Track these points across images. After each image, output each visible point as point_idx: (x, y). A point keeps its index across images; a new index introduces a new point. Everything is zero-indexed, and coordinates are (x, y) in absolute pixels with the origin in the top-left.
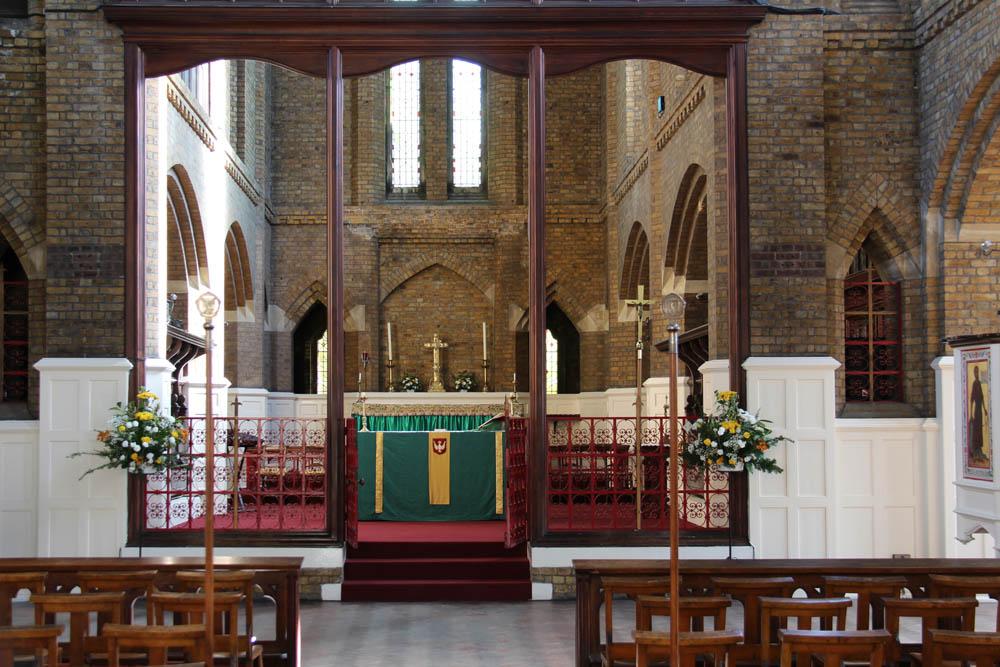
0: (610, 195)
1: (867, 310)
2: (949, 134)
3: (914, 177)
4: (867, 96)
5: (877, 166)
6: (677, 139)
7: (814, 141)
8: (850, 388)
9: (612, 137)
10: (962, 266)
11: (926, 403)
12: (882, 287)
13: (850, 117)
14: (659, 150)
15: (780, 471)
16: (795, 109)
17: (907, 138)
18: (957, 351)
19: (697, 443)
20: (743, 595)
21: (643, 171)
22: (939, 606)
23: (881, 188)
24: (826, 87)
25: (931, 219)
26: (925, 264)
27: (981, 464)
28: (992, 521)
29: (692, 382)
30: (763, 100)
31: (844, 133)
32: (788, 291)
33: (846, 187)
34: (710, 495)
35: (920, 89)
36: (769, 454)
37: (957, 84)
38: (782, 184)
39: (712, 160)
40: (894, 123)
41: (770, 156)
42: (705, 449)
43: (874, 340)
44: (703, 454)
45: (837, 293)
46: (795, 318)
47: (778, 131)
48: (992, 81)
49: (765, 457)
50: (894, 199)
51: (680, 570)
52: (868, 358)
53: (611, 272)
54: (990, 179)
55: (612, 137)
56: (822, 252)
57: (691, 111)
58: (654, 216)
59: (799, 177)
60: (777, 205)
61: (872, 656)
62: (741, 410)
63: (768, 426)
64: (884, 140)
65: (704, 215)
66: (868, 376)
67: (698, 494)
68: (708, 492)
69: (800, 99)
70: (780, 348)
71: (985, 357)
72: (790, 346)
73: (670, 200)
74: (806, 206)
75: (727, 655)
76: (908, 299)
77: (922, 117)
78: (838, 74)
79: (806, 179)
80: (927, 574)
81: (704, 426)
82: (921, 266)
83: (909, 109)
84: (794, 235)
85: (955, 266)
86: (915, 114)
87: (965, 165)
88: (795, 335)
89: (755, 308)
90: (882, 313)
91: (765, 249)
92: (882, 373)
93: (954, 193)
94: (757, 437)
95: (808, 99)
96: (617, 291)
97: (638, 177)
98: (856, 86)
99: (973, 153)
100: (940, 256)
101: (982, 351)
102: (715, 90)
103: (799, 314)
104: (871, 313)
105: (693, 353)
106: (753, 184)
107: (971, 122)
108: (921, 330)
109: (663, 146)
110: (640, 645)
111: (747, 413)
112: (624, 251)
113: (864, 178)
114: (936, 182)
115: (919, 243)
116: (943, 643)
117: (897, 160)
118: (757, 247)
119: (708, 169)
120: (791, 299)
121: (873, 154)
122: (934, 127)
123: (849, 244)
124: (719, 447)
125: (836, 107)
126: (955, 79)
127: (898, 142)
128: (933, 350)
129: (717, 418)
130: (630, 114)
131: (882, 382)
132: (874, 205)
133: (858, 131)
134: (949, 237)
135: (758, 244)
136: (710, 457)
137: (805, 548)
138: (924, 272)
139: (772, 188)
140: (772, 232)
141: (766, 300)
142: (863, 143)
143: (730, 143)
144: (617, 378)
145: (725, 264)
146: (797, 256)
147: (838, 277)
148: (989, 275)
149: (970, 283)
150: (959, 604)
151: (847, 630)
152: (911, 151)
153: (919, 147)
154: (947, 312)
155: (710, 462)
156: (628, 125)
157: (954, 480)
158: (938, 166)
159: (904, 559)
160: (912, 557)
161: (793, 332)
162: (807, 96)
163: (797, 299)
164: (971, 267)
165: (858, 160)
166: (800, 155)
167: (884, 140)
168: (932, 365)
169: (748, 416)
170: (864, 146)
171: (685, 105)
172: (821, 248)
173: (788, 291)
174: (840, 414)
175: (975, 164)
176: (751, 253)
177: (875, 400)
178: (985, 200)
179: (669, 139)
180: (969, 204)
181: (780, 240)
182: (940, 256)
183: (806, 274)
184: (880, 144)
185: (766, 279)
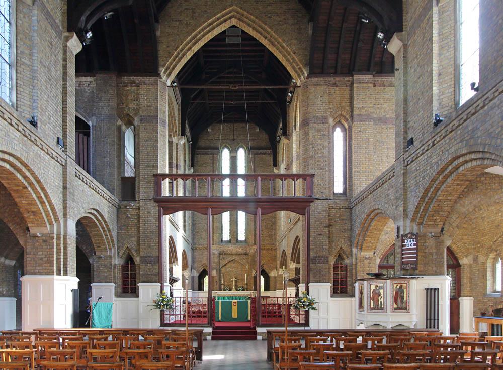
3: (350, 239)
6: (293, 230)
25: (354, 250)
36: (314, 306)
64: (343, 231)
73: (292, 245)
74: (324, 247)
85: (360, 261)
100: (356, 259)
108: (352, 277)
119: (301, 237)
131: (341, 289)
134: (358, 254)
152: (349, 233)
167: (343, 231)
172: (327, 257)
174: (332, 297)
182: (356, 259)
183: (324, 263)
185: (314, 265)
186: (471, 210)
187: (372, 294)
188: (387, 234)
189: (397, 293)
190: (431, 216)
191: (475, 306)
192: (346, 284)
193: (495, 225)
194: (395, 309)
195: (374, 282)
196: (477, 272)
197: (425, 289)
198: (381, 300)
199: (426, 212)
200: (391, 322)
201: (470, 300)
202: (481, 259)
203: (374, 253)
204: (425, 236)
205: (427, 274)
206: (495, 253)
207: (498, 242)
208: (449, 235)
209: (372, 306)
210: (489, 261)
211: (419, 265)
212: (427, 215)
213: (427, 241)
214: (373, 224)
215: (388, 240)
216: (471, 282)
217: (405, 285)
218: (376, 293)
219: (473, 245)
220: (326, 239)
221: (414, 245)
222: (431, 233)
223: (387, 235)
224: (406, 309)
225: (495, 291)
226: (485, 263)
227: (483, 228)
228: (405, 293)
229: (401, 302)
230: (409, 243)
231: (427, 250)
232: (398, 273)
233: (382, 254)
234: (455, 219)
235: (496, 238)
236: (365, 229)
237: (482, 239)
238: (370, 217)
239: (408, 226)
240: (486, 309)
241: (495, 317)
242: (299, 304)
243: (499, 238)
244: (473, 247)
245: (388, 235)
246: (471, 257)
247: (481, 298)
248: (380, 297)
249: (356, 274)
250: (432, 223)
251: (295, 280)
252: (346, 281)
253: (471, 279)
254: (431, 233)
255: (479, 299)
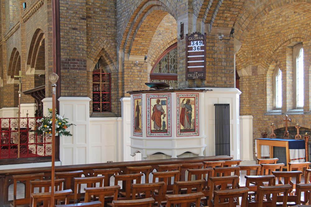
0: (3, 37)
1: (100, 82)
2: (126, 26)
3: (115, 37)
4: (100, 11)
5: (103, 34)
6: (32, 19)
7: (83, 24)
8: (94, 107)
9: (4, 15)
10: (130, 69)
11: (118, 112)
12: (104, 75)
13: (95, 17)
14: (24, 22)
15: (71, 135)
16: (76, 13)
17: (113, 26)
18: (131, 95)
19: (41, 126)
20: (24, 182)
21: (17, 29)
22: (132, 176)
23: (105, 42)
24: (87, 6)
25: (120, 53)
26: (118, 68)
27: (138, 131)
28: (142, 149)
29: (37, 105)
30: (65, 8)
31: (93, 23)
32: (74, 75)
33: (93, 41)
34: (46, 144)
35: (117, 10)
36: (67, 130)
37: (129, 10)
38: (72, 38)
39: (47, 28)
40: (109, 21)
41: (68, 28)
42: (45, 128)
43: (102, 92)
44: (44, 130)
45: (90, 76)
46: (76, 84)
47: (70, 20)
48: (140, 10)
49: (66, 131)
50: (109, 46)
51: (55, 170)
52: (100, 98)
53: (4, 66)
54: (138, 41)
55: (4, 15)
56: (85, 62)
57: (37, 10)
58: (23, 46)
59: (78, 36)
60: (70, 45)
61: (114, 194)
62: (58, 115)
63: (67, 120)
64: (106, 26)
65: (43, 47)
66: (100, 103)
67: (41, 144)
68: (45, 143)
69: (78, 9)
70: (71, 94)
71: (140, 98)
72: (75, 93)
73: (29, 41)
74: (80, 46)
75: (66, 198)
76: (113, 79)
77: (117, 20)
78: (91, 2)
79: (80, 37)
80: (126, 167)
81: (44, 121)
82: (117, 68)
83: (113, 17)
84: (76, 56)
85: (128, 68)
86: (115, 18)
87: (131, 36)
88: (76, 90)
89: (62, 80)
90: (104, 83)
91: (66, 60)
92: (104, 102)
93: (127, 45)
94: (63, 124)
95: (81, 10)
96: (7, 72)
97: (15, 31)
98: (97, 7)
99: (134, 32)
100: (123, 65)
101: (139, 96)
102: (48, 3)
103: (78, 82)
104: (101, 83)
105: (38, 95)
106: (62, 37)
107: (133, 23)
108: (117, 89)
109: (26, 21)
110: (34, 198)
111: (60, 116)
112: (9, 58)
113: (99, 38)
114: (122, 41)
115: (117, 61)
116: (136, 188)
117: (110, 33)
118: (64, 59)
119: (45, 30)
120: (75, 77)
121: (102, 30)
122: (121, 23)
123: (94, 60)
124: (50, 128)
125: (90, 13)
126: (128, 8)
127: (110, 27)
128: (121, 95)
129: (49, 118)
130: (11, 7)
131: (104, 105)
132: (103, 48)
133: (97, 22)
134: (126, 59)
135: (64, 58)
136: (46, 131)
137: (79, 160)
138: (118, 70)
139: (69, 39)
140: (69, 54)
141: (66, 77)
142: (99, 26)
143: (53, 23)
144: (6, 104)
145: (52, 64)
146: (77, 63)
147: (90, 71)
148: (138, 72)
149: (132, 74)
150: (138, 175)
151: (111, 185)
152: (113, 30)
153: (117, 29)
154: (125, 83)
155: (46, 133)
156: (10, 11)
157: (130, 136)
158: (123, 36)
159: (111, 162)
160: (113, 162)
161: (75, 89)
162: (80, 9)
163: (77, 77)
164: (132, 69)
165: (97, 32)
166: (78, 29)
167: (106, 26)
168: (120, 100)
169: (60, 117)
170: (99, 28)
171: (35, 7)
172: (85, 61)
173: (74, 75)
174: (91, 116)
175: (134, 36)
176: (61, 61)
177: (102, 111)
178: (137, 48)
179: (28, 19)
180: (132, 49)
181: (71, 57)
182: (123, 65)
183: (80, 69)
184: (104, 27)
185: (67, 70)
186: (261, 9)
187: (152, 112)
188: (160, 34)
189: (183, 110)
190: (221, 12)
191: (254, 126)
192: (110, 99)
193: (275, 31)
194: (181, 131)
195: (156, 95)
196: (257, 86)
197: (215, 105)
198: (164, 119)
199: (216, 7)
200: (177, 149)
201: (250, 119)
202: (261, 71)
203: (145, 59)
204: (213, 38)
205: (216, 86)
206: (275, 64)
207: (278, 51)
208: (239, 38)
209: (153, 129)
210: (268, 72)
211: (207, 74)
212: (217, 11)
213: (216, 44)
214: (145, 19)
215: (162, 42)
216: (250, 98)
217: (193, 99)
218: (158, 111)
219: (252, 54)
220: (82, 35)
221: (202, 48)
222: (220, 34)
223: (166, 31)
224: (166, 131)
225: (275, 108)
226: (264, 75)
227: (263, 35)
228: (193, 110)
229: (188, 122)
230: (195, 45)
231: (215, 56)
232: (182, 84)
233: (154, 61)
234: (244, 19)
235: (275, 47)
236: (135, 26)
237: (261, 47)
238: (142, 10)
239: (193, 24)
240: (267, 129)
241: (277, 138)
242: (44, 127)
243: (279, 47)
244: (252, 56)
245: (161, 36)
246: (249, 68)
247: (261, 117)
248: (162, 116)
249: (123, 85)
250: (221, 22)
251: (36, 92)
252: (110, 94)
253: (250, 94)
254: (220, 34)
255: (259, 117)
